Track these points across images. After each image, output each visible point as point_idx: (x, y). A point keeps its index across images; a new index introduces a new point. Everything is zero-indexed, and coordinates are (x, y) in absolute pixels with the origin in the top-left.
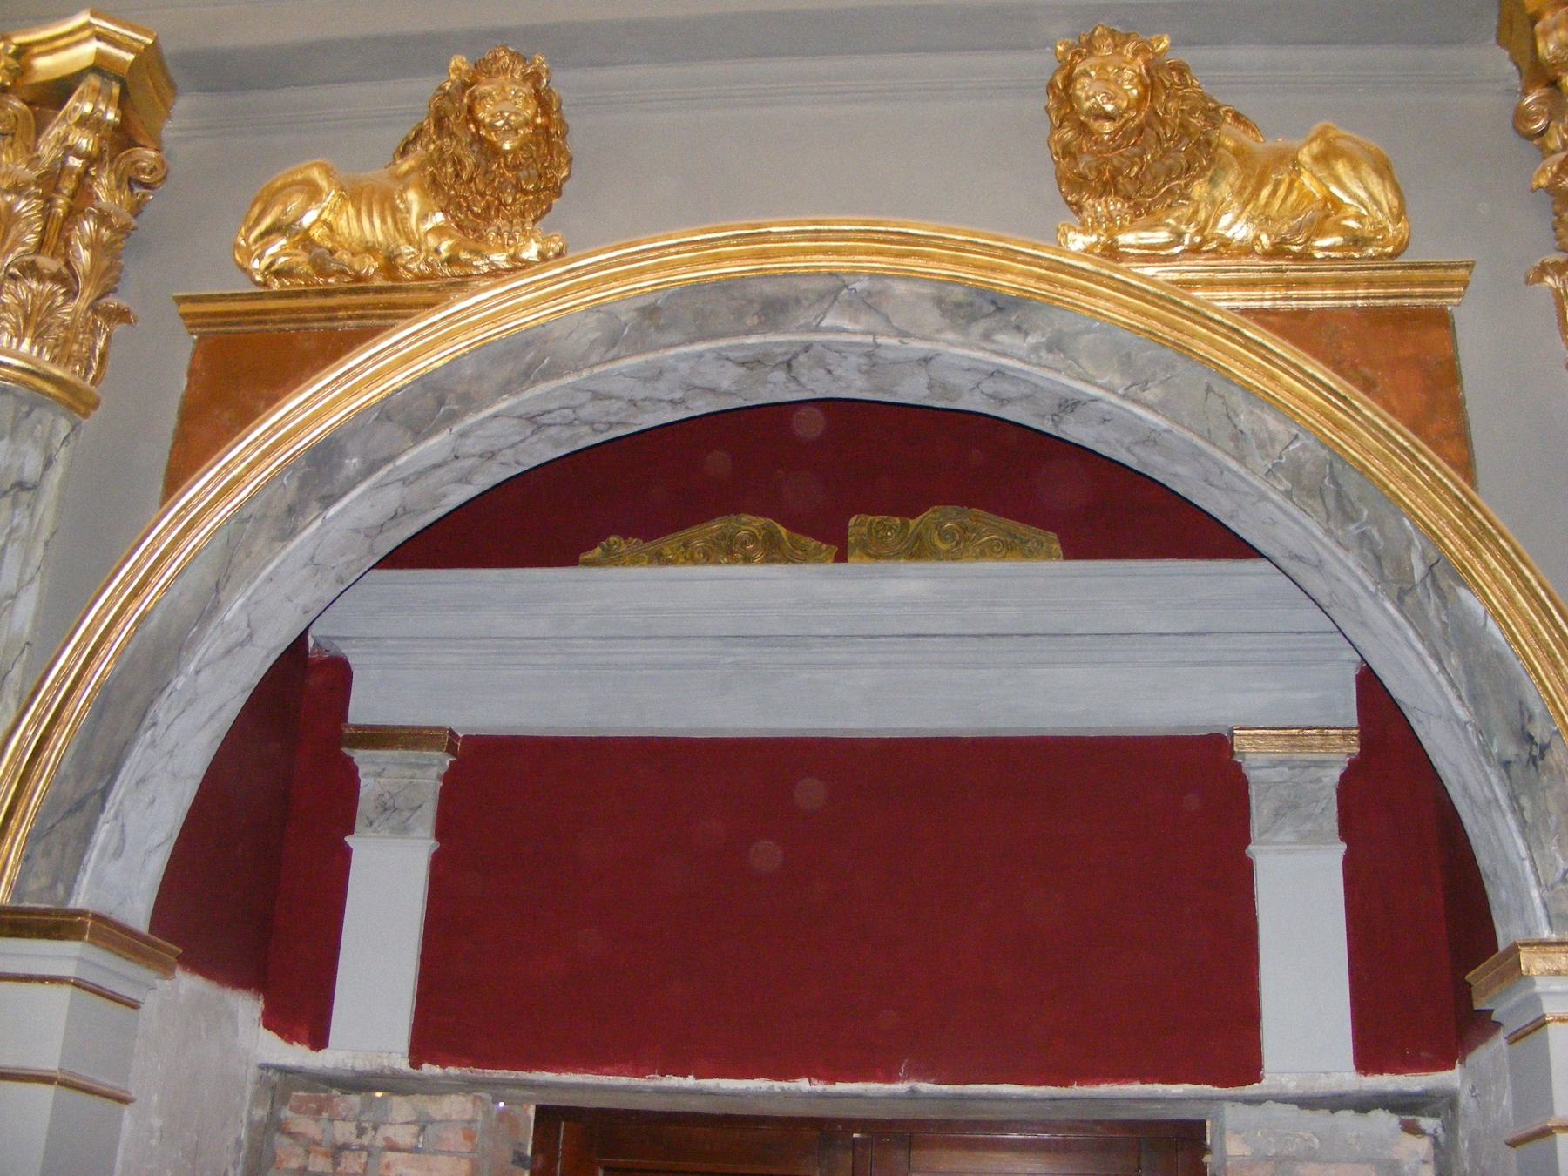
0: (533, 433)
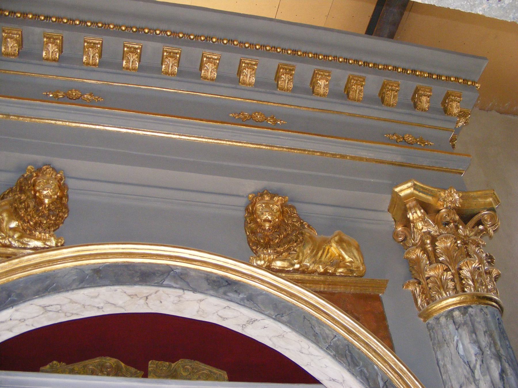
0: (43, 314)
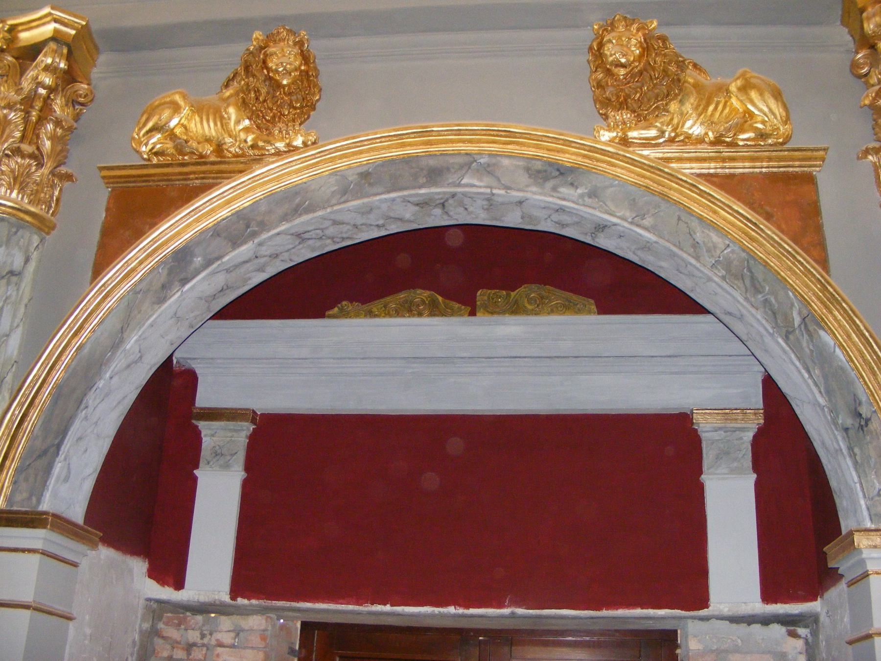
0: (300, 243)
